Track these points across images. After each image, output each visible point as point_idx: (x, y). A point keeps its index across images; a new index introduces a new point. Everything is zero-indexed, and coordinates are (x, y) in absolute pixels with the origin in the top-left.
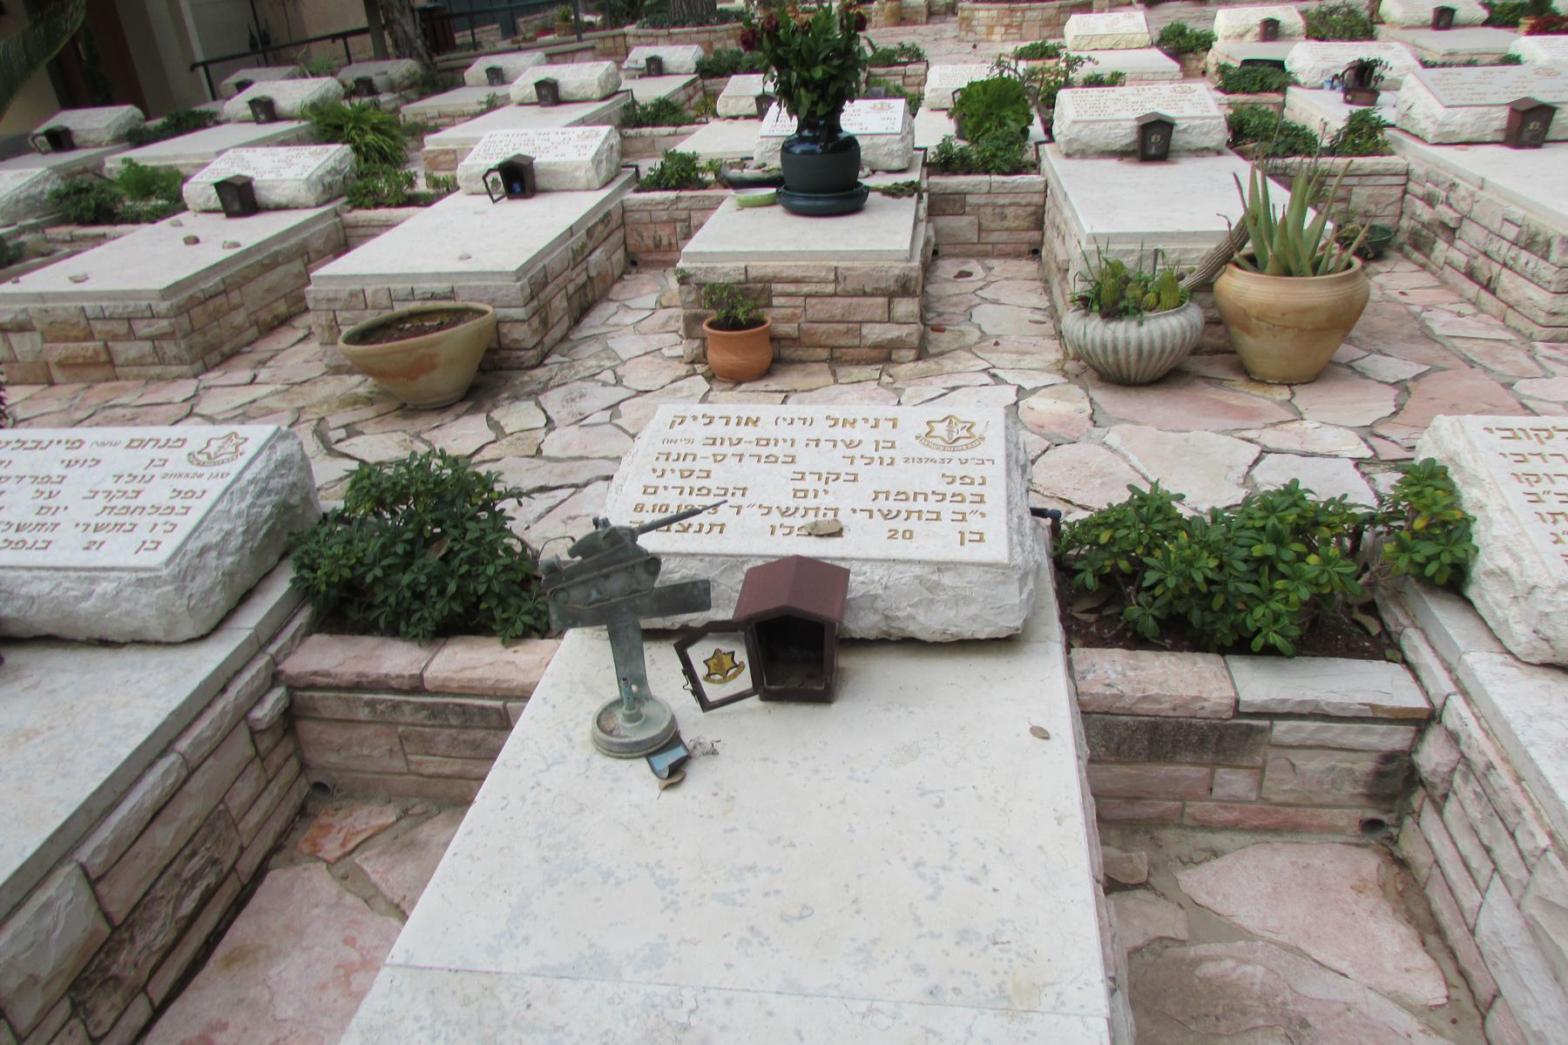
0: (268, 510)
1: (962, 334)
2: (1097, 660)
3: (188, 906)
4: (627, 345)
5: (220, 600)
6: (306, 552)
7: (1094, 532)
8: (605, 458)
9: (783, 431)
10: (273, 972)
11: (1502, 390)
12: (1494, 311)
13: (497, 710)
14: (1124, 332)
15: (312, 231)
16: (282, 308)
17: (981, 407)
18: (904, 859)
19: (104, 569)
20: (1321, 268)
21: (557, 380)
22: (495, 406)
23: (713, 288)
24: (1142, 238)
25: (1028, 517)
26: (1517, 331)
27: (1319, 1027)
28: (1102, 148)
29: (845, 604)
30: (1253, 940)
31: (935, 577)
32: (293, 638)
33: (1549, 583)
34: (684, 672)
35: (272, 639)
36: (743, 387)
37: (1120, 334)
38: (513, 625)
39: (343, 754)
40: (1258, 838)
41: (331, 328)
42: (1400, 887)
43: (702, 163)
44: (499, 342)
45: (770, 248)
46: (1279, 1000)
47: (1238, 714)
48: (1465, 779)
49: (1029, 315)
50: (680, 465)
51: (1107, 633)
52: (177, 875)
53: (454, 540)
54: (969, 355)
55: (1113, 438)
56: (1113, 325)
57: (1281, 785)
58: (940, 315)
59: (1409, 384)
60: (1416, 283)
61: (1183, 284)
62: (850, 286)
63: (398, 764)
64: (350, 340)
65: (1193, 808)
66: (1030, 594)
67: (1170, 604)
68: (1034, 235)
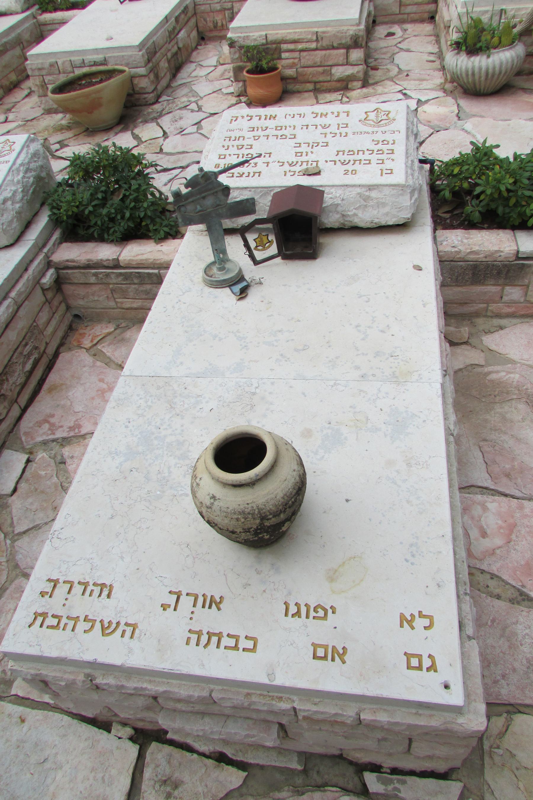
0: (32, 180)
1: (388, 70)
3: (28, 367)
4: (202, 88)
5: (16, 226)
6: (54, 201)
7: (451, 168)
9: (289, 122)
10: (70, 394)
13: (156, 274)
14: (480, 62)
15: (22, 28)
16: (13, 77)
17: (398, 109)
22: (135, 127)
23: (248, 49)
25: (417, 163)
29: (323, 210)
30: (515, 364)
32: (54, 245)
34: (245, 246)
35: (44, 246)
37: (477, 64)
38: (159, 233)
39: (86, 300)
40: (523, 320)
41: (42, 86)
44: (133, 90)
45: (279, 22)
47: (518, 258)
49: (426, 57)
50: (237, 143)
51: (455, 223)
52: (21, 353)
53: (126, 190)
55: (468, 126)
56: (472, 59)
58: (376, 60)
61: (515, 31)
62: (325, 43)
63: (112, 304)
64: (54, 92)
65: (493, 307)
66: (416, 200)
67: (488, 205)
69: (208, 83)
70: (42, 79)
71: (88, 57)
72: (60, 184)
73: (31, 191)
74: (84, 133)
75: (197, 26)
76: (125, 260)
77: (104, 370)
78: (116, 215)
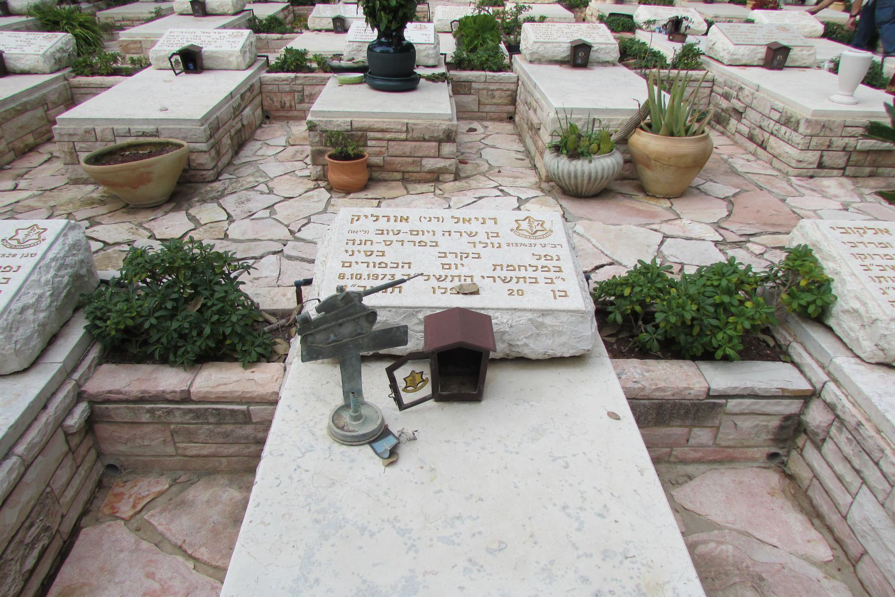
1: (478, 165)
2: (625, 366)
3: (30, 563)
4: (272, 169)
5: (37, 343)
7: (619, 288)
8: (271, 240)
9: (425, 226)
11: (780, 203)
12: (765, 159)
13: (243, 412)
14: (581, 166)
15: (49, 89)
16: (30, 140)
18: (555, 505)
20: (689, 132)
21: (230, 190)
24: (590, 111)
26: (779, 170)
27: (770, 580)
28: (550, 58)
31: (540, 320)
32: (90, 367)
33: (885, 318)
35: (75, 369)
36: (352, 195)
38: (250, 354)
39: (129, 445)
41: (71, 153)
42: (793, 492)
43: (310, 56)
44: (189, 165)
46: (744, 565)
47: (709, 396)
48: (840, 430)
50: (363, 248)
51: (624, 350)
52: (21, 542)
54: (485, 179)
56: (574, 162)
57: (727, 436)
59: (732, 199)
60: (721, 142)
61: (613, 138)
62: (416, 135)
64: (88, 161)
65: (677, 451)
68: (510, 108)
69: (277, 163)
70: (72, 145)
72: (104, 282)
73: (63, 295)
74: (123, 210)
75: (262, 104)
76: (199, 392)
77: (155, 557)
78: (191, 331)
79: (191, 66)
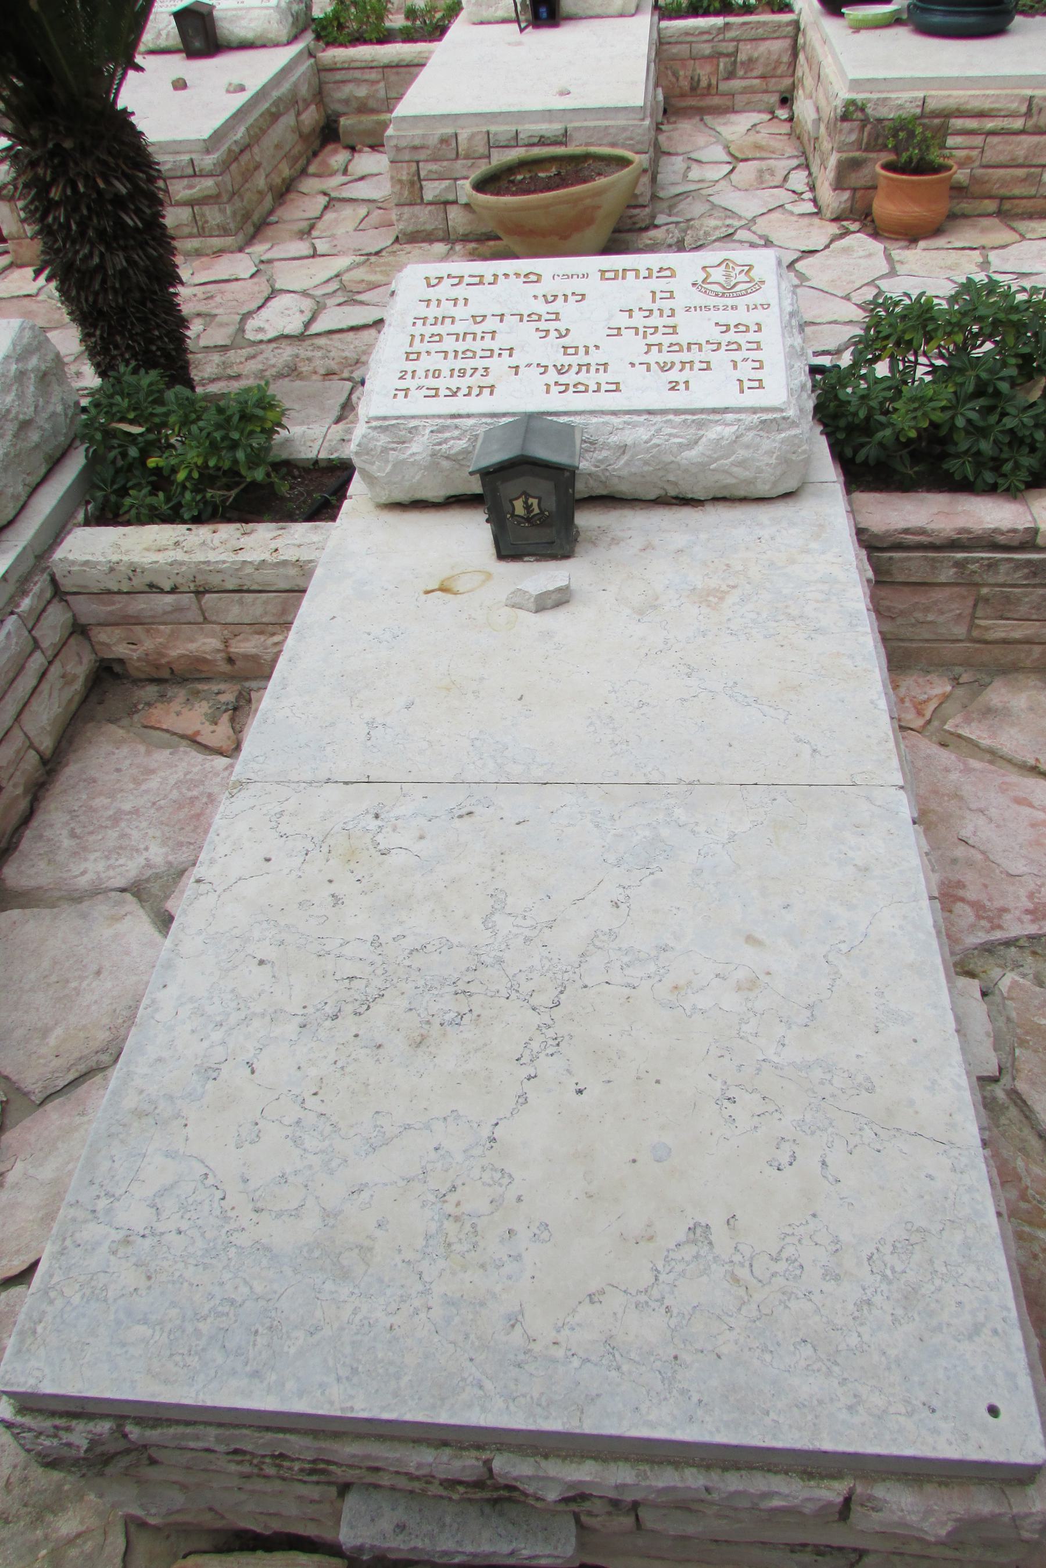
8: (835, 322)
19: (714, 411)
36: (922, 244)
39: (900, 621)
71: (527, 127)
79: (543, 11)
